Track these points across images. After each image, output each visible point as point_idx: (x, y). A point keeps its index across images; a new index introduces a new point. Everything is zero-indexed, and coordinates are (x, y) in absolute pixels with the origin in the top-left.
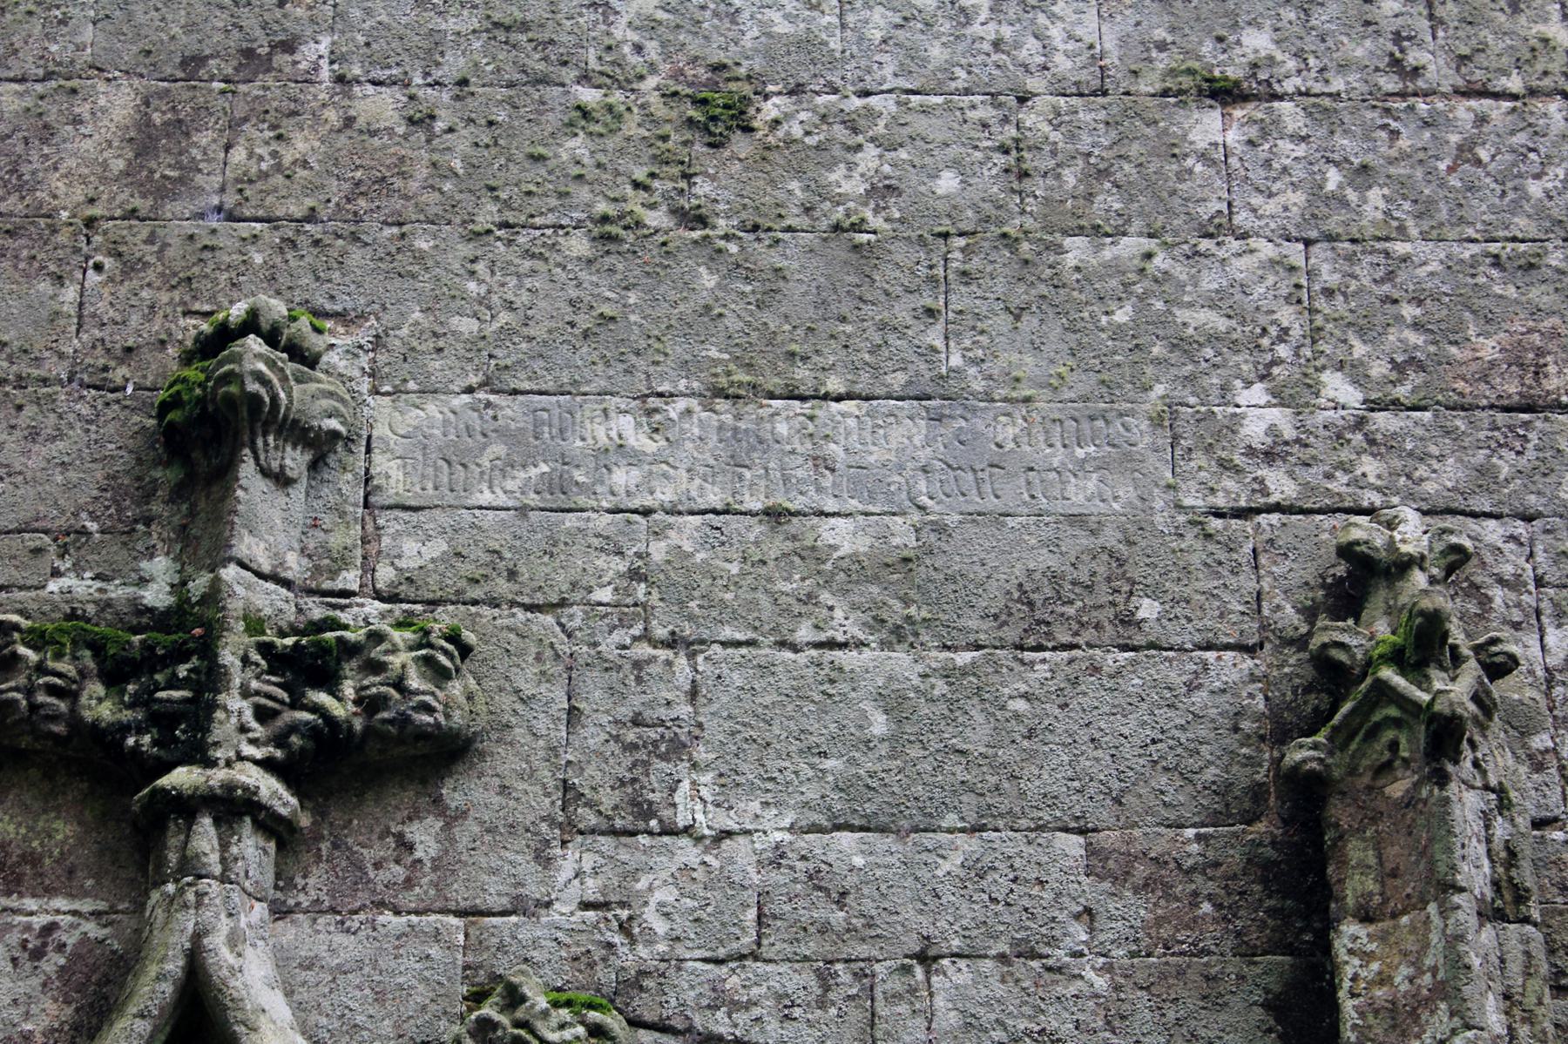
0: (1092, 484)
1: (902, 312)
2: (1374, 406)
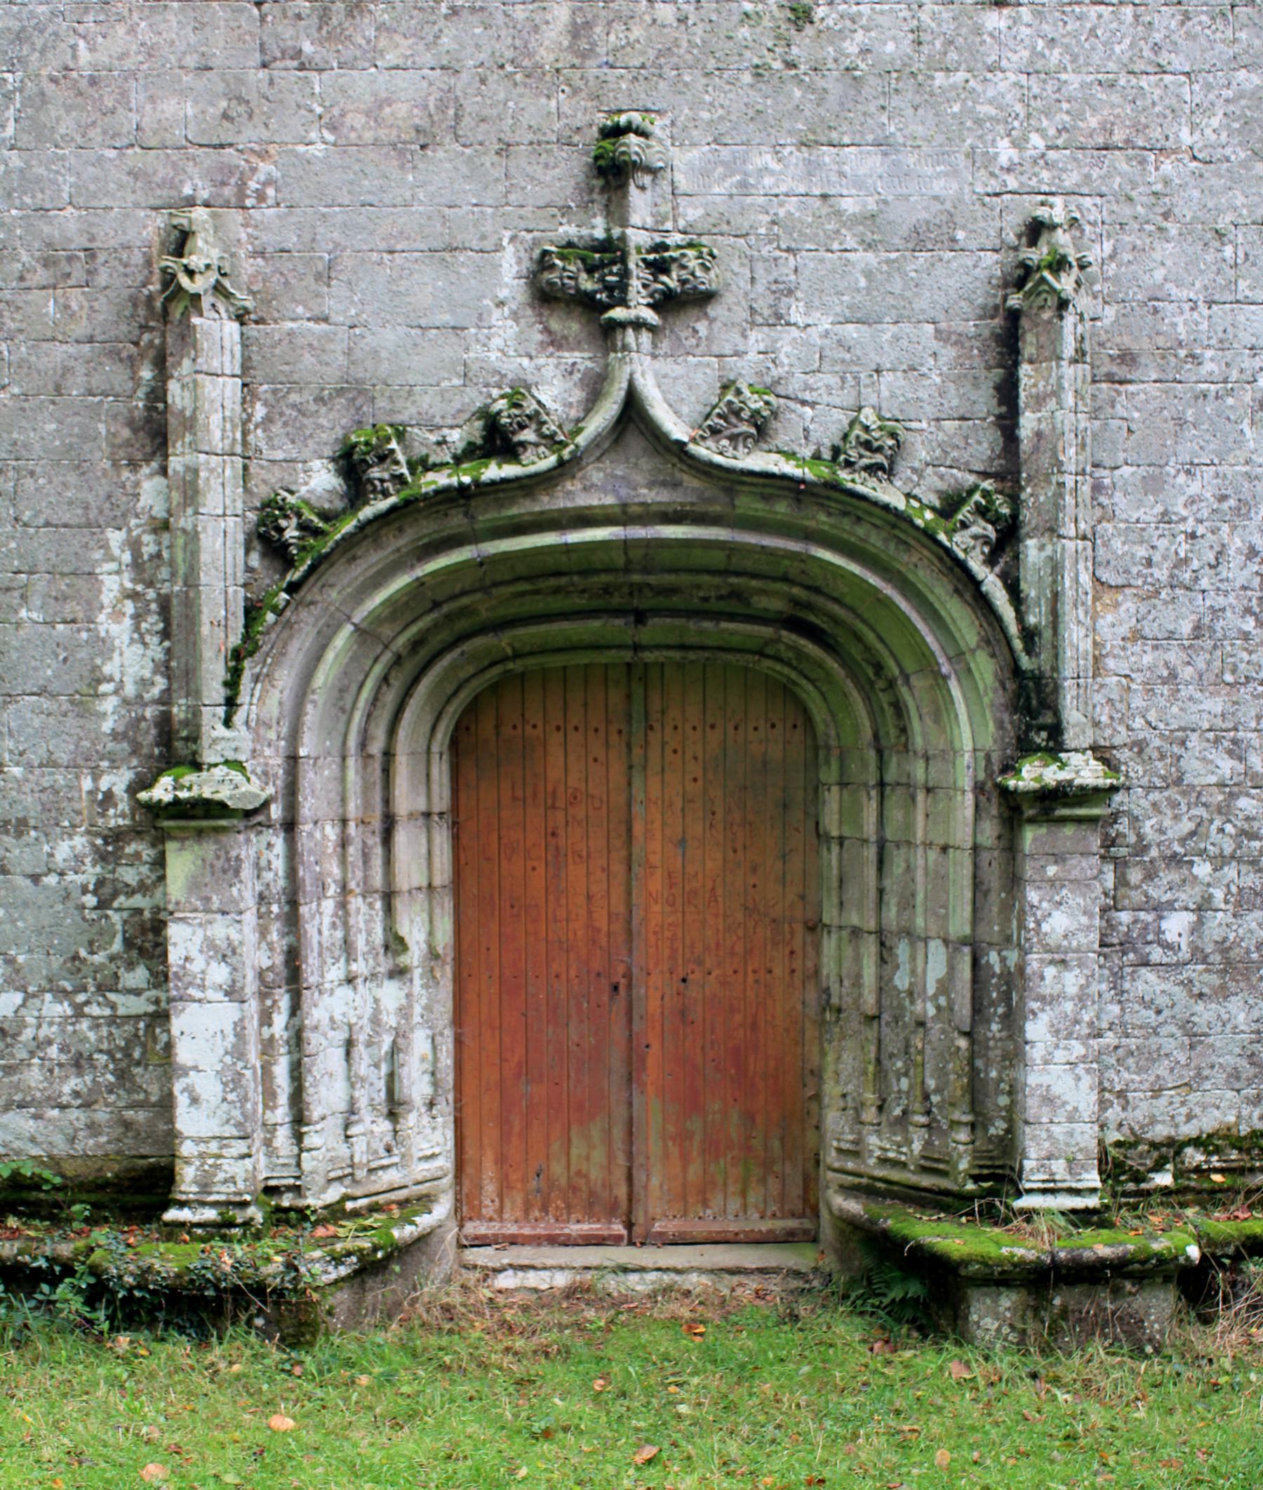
0: (942, 183)
2: (1049, 148)
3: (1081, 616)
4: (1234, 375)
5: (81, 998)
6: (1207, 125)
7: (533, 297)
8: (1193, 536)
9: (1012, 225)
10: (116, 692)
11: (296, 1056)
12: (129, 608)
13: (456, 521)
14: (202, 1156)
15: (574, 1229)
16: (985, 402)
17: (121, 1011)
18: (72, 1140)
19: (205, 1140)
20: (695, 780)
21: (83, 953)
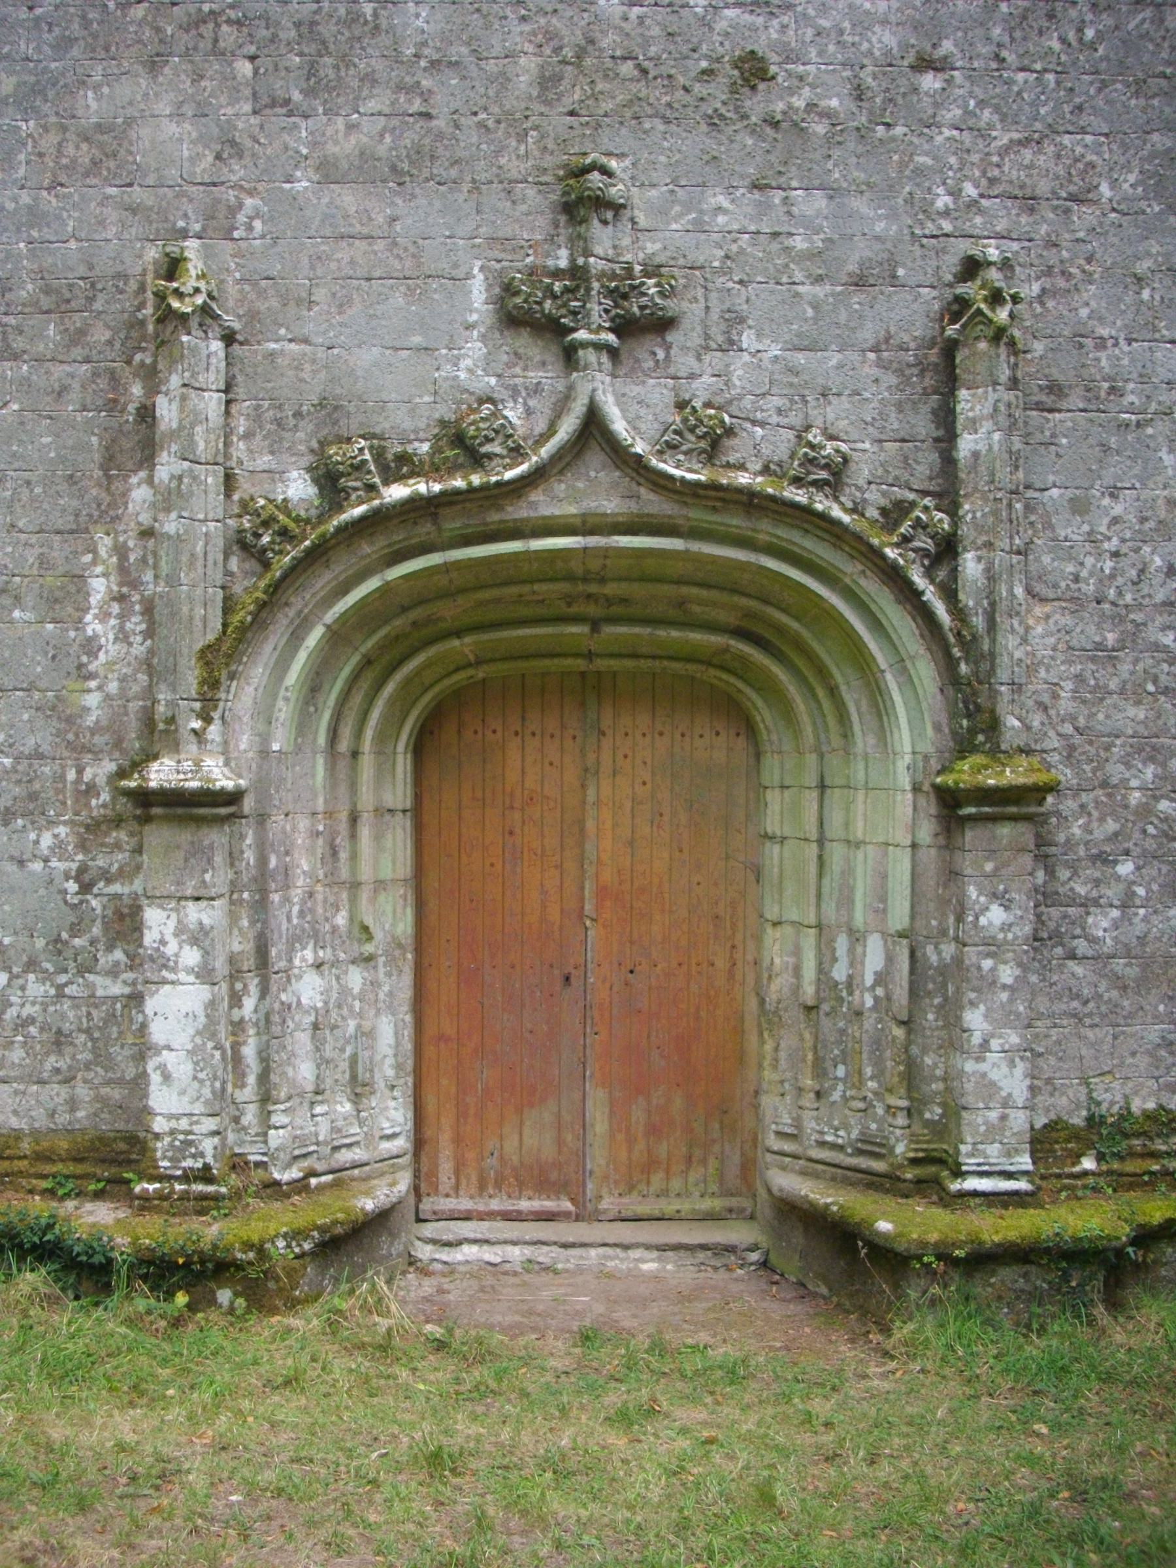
0: (883, 225)
1: (817, 156)
2: (982, 196)
3: (1016, 625)
4: (1153, 407)
5: (62, 979)
6: (1126, 181)
7: (500, 321)
8: (1116, 554)
9: (950, 264)
10: (100, 688)
11: (265, 1038)
12: (115, 608)
13: (425, 530)
14: (172, 1132)
15: (524, 1205)
16: (923, 425)
17: (100, 993)
18: (52, 1114)
19: (178, 1117)
20: (644, 783)
21: (64, 935)
